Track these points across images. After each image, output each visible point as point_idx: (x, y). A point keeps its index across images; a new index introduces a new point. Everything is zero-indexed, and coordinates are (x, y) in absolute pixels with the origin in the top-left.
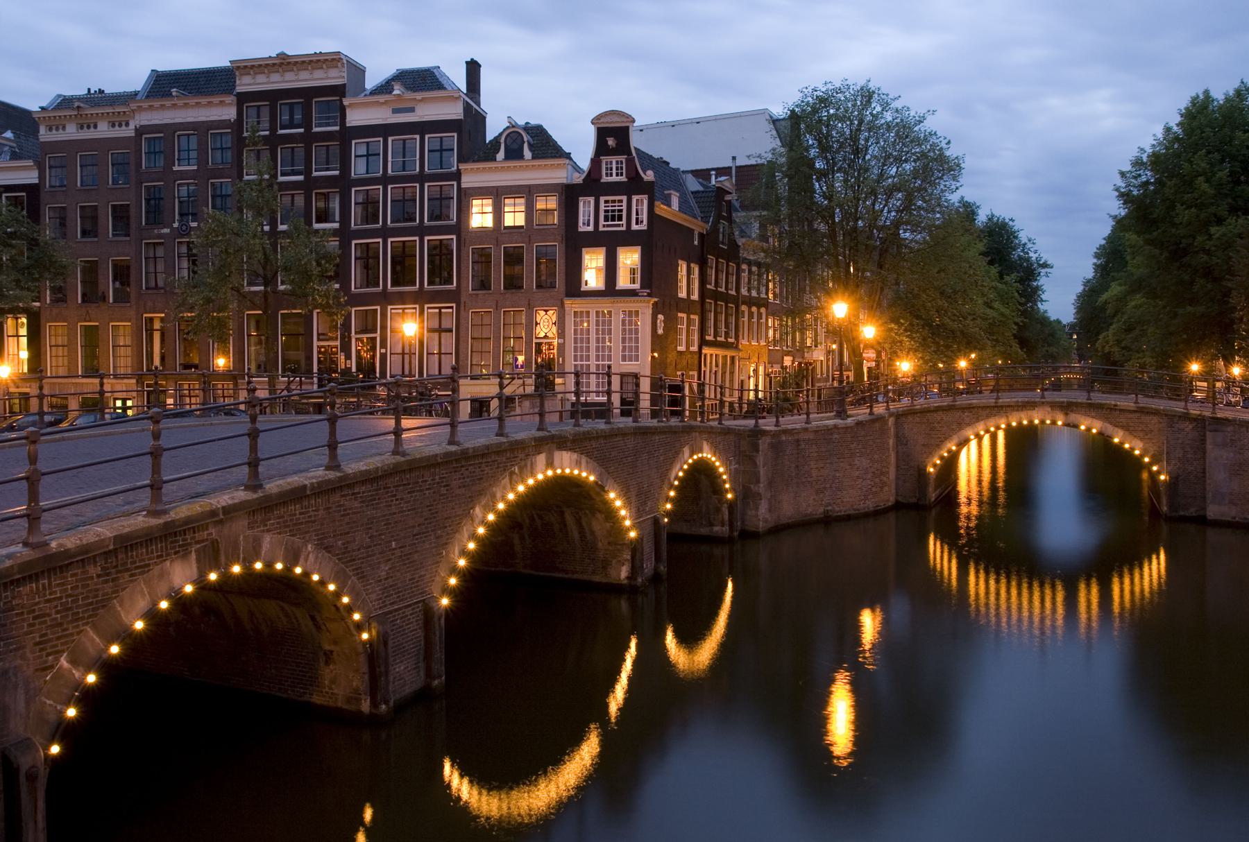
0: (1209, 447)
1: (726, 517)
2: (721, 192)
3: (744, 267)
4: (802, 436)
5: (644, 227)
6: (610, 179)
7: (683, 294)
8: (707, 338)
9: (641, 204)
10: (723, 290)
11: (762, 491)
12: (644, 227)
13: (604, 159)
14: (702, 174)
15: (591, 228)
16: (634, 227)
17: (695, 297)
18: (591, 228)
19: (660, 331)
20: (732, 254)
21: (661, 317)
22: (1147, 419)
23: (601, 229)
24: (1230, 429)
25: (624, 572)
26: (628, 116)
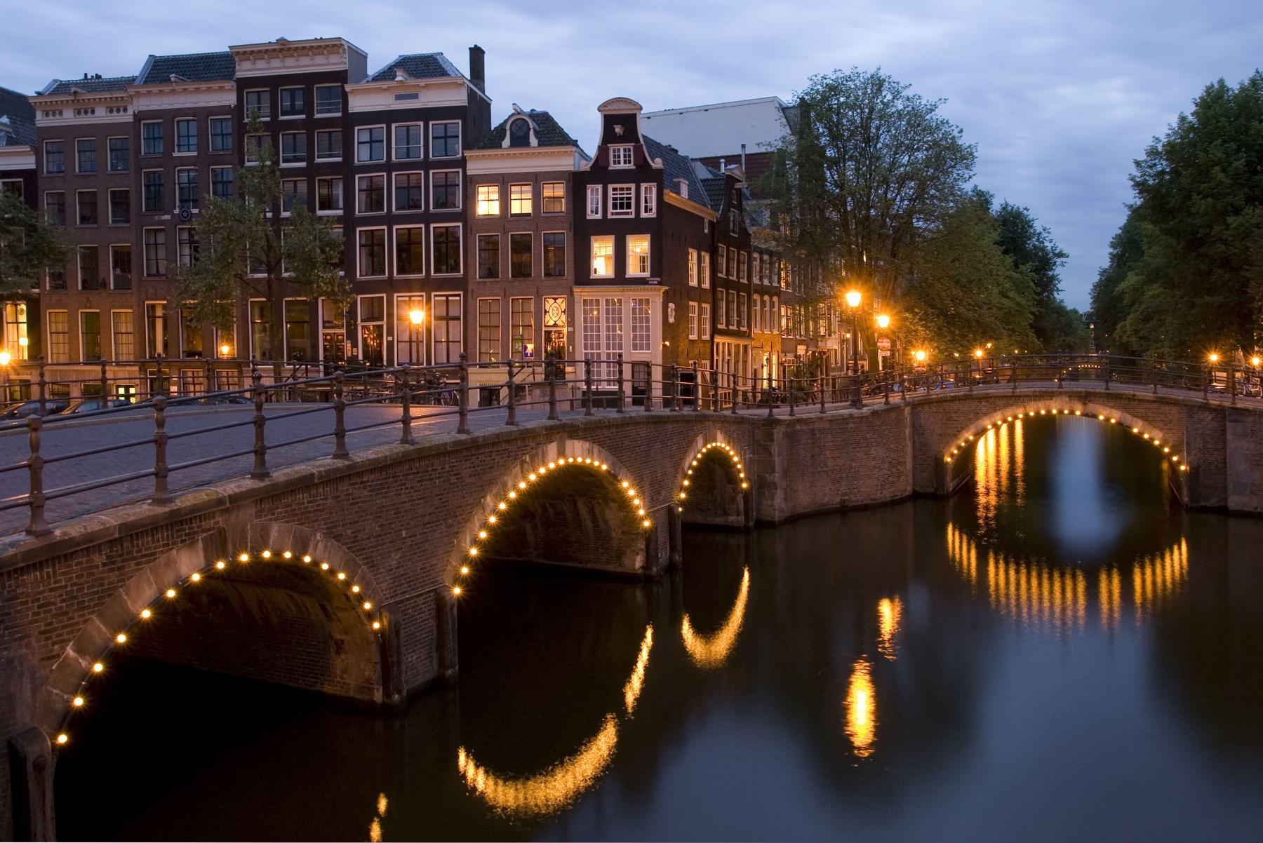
0: (1229, 437)
1: (741, 507)
2: (730, 180)
3: (756, 255)
4: (817, 426)
5: (653, 215)
6: (617, 167)
7: (694, 283)
8: (719, 326)
9: (649, 192)
10: (734, 278)
11: (776, 480)
12: (653, 215)
13: (612, 147)
14: (711, 162)
15: (599, 216)
16: (643, 215)
17: (706, 285)
18: (599, 216)
19: (671, 320)
20: (743, 242)
21: (671, 305)
22: (1166, 409)
23: (610, 217)
24: (1251, 419)
25: (639, 562)
26: (636, 104)
